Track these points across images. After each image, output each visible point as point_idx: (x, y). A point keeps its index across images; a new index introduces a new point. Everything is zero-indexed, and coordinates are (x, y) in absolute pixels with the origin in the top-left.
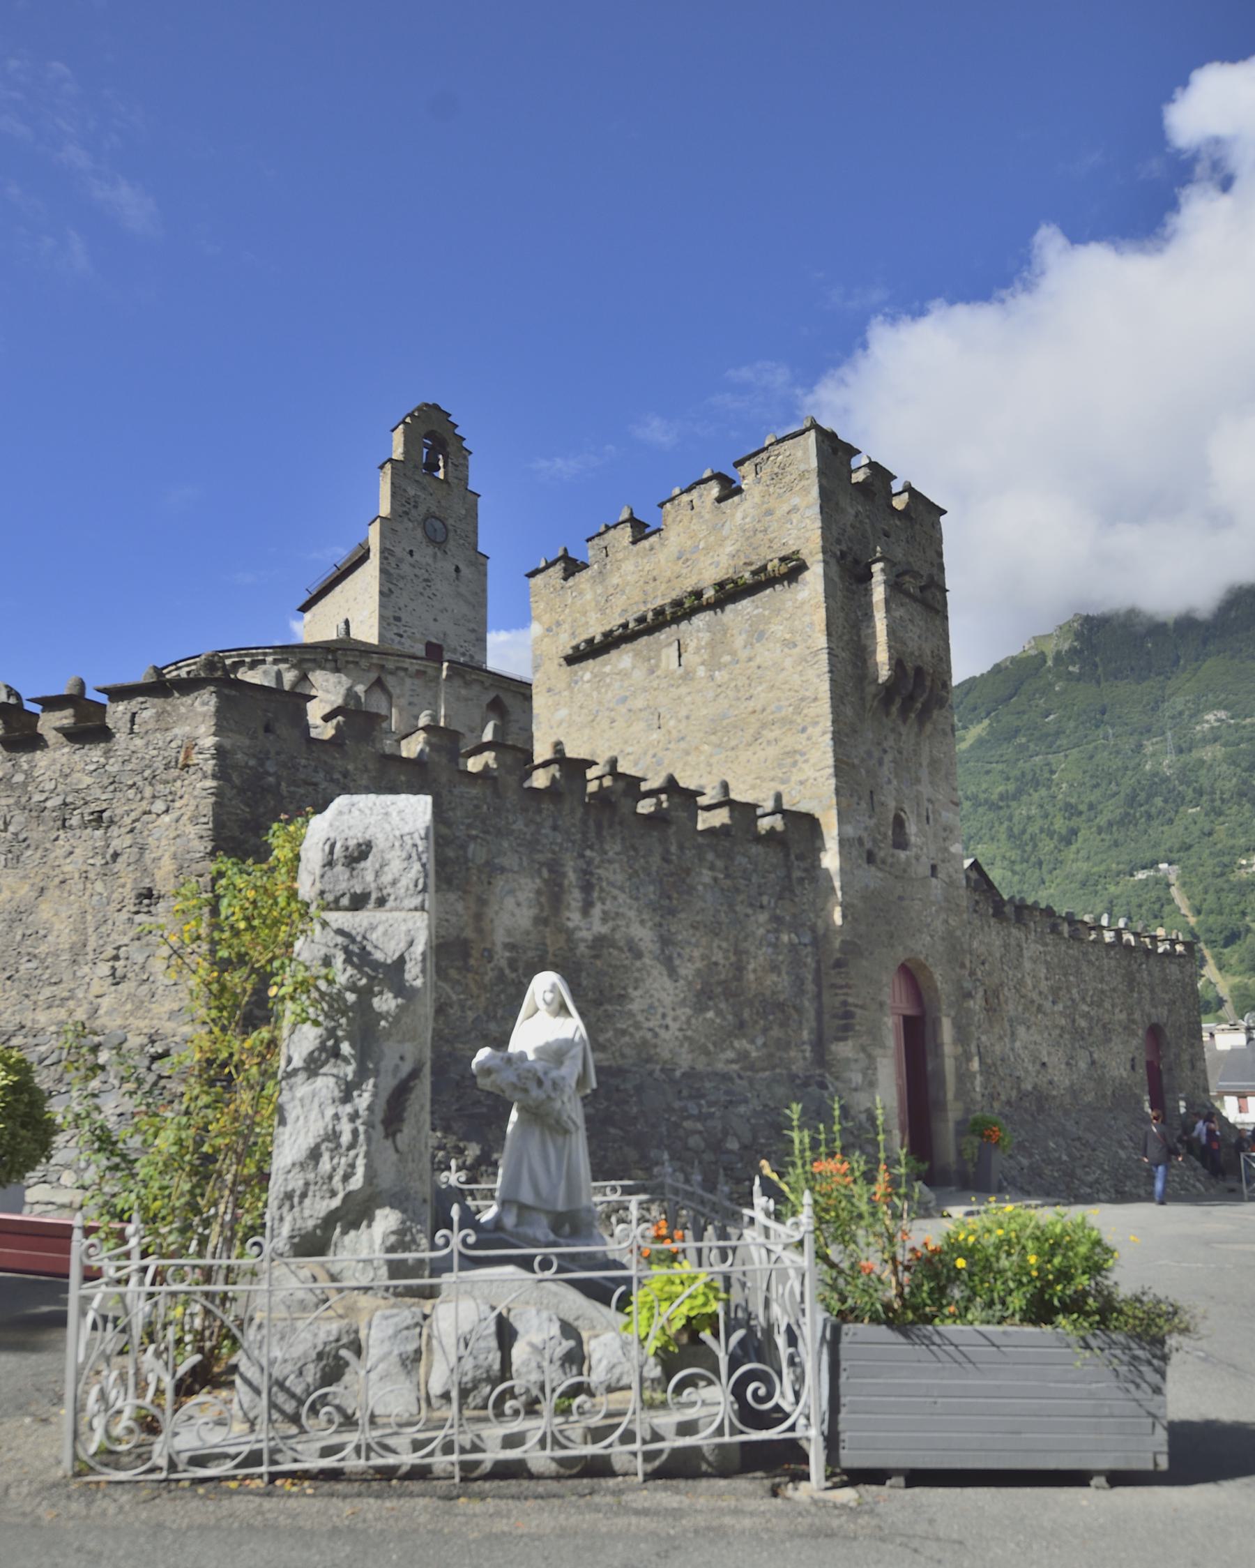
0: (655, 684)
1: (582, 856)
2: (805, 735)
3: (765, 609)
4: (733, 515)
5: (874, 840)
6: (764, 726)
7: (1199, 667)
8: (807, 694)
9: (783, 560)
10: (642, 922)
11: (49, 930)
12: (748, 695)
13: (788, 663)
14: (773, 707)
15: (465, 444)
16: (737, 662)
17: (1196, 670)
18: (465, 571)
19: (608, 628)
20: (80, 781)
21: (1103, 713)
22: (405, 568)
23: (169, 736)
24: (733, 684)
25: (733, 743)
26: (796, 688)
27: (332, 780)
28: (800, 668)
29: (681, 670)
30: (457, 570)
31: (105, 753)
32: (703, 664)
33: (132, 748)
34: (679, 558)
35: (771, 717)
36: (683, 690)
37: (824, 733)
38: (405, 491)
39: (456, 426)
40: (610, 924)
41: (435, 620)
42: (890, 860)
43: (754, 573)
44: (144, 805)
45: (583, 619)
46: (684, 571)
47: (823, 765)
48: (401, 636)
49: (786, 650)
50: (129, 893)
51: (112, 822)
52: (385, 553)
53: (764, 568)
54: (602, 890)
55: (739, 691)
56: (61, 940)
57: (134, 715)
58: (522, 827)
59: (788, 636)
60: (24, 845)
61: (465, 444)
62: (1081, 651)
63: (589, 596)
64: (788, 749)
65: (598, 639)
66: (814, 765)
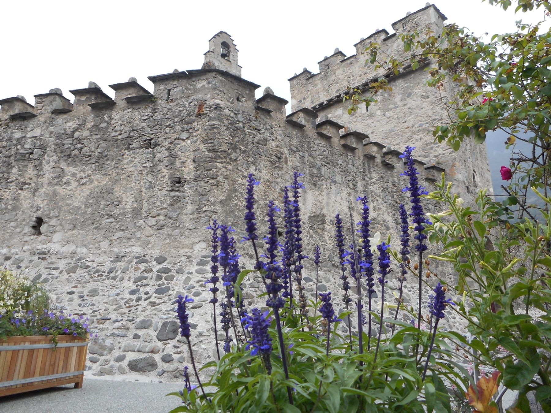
0: (354, 120)
1: (364, 179)
3: (411, 83)
4: (392, 46)
5: (469, 183)
8: (436, 117)
10: (388, 213)
11: (120, 202)
13: (425, 105)
14: (418, 125)
16: (397, 107)
19: (330, 98)
20: (138, 125)
23: (190, 100)
24: (396, 117)
25: (397, 142)
26: (430, 115)
27: (266, 129)
29: (368, 113)
31: (152, 110)
32: (379, 109)
33: (169, 107)
34: (365, 66)
36: (370, 121)
40: (377, 212)
42: (473, 192)
43: (404, 69)
44: (176, 136)
45: (317, 96)
46: (368, 71)
49: (423, 100)
50: (166, 181)
51: (156, 145)
54: (373, 197)
55: (399, 119)
56: (127, 206)
57: (169, 91)
58: (341, 163)
59: (424, 94)
60: (105, 158)
61: (236, 47)
63: (320, 86)
64: (427, 142)
65: (325, 103)
66: (442, 148)
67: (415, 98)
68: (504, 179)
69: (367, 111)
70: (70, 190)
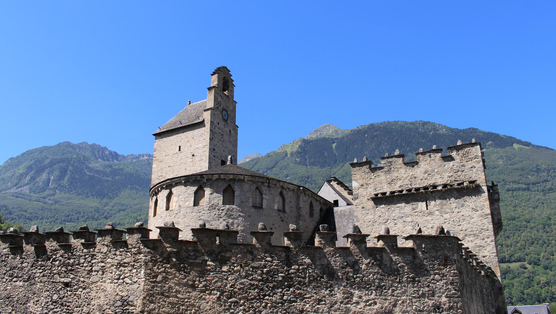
2: (484, 241)
6: (466, 235)
7: (344, 165)
8: (484, 228)
9: (470, 182)
12: (459, 224)
14: (470, 230)
15: (233, 83)
17: (342, 166)
18: (232, 132)
21: (308, 178)
22: (216, 129)
28: (480, 219)
29: (428, 211)
30: (230, 131)
35: (469, 233)
36: (429, 218)
37: (492, 241)
38: (217, 99)
39: (232, 76)
41: (224, 151)
43: (459, 184)
47: (492, 252)
48: (215, 157)
49: (474, 212)
52: (212, 123)
53: (463, 183)
59: (474, 207)
62: (301, 153)
67: (467, 209)
68: (204, 126)
69: (427, 209)
70: (360, 309)
